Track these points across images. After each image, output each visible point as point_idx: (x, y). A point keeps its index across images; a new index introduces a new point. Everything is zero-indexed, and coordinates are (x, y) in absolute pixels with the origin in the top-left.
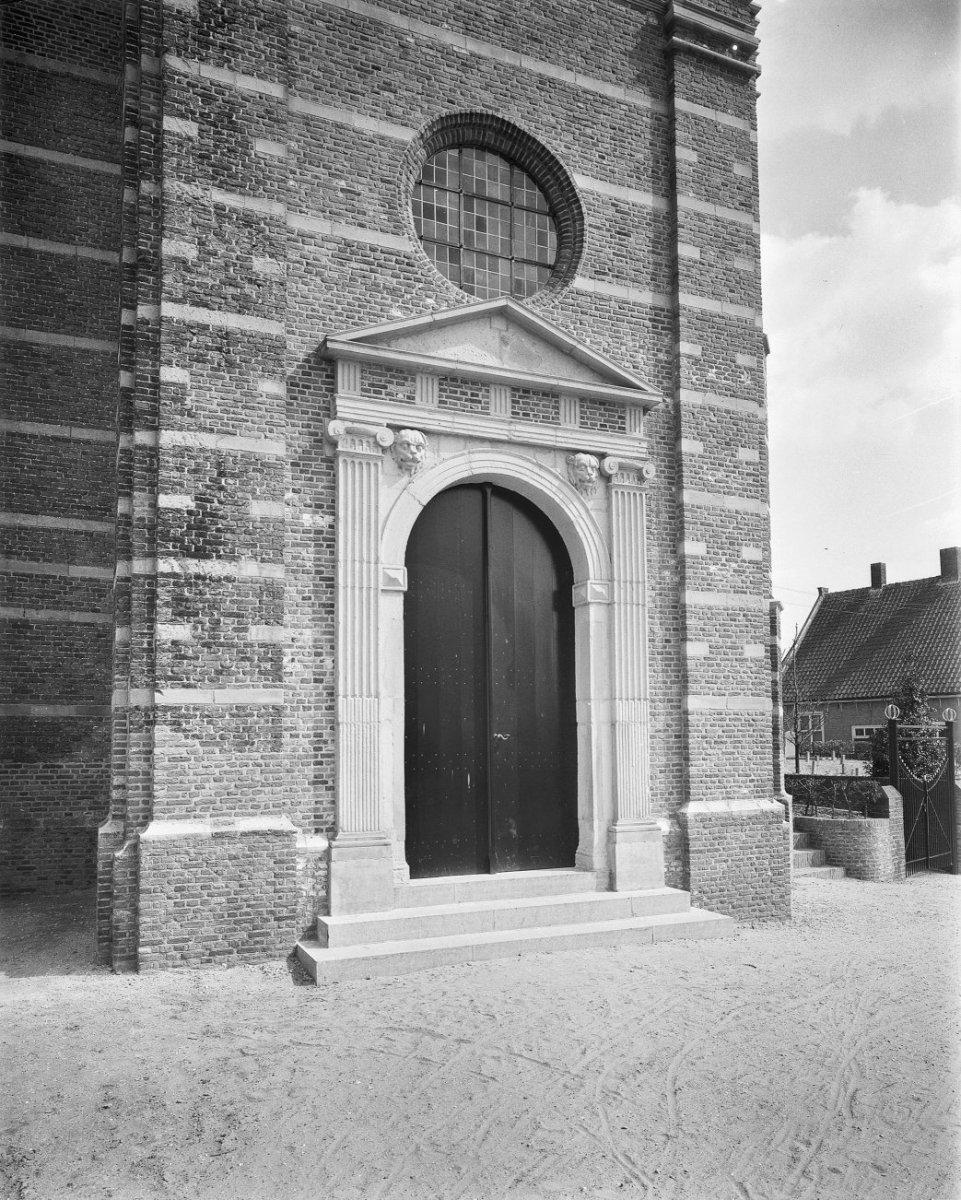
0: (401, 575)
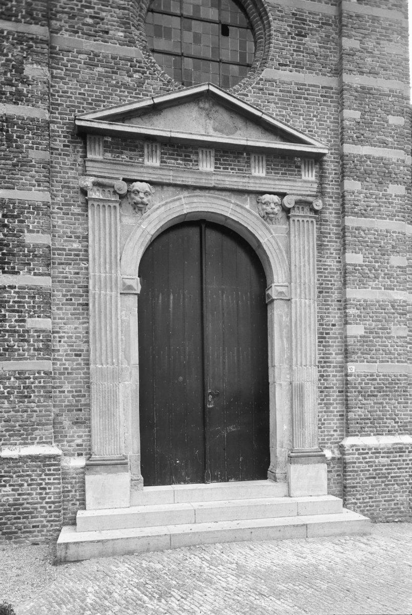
0: (136, 284)
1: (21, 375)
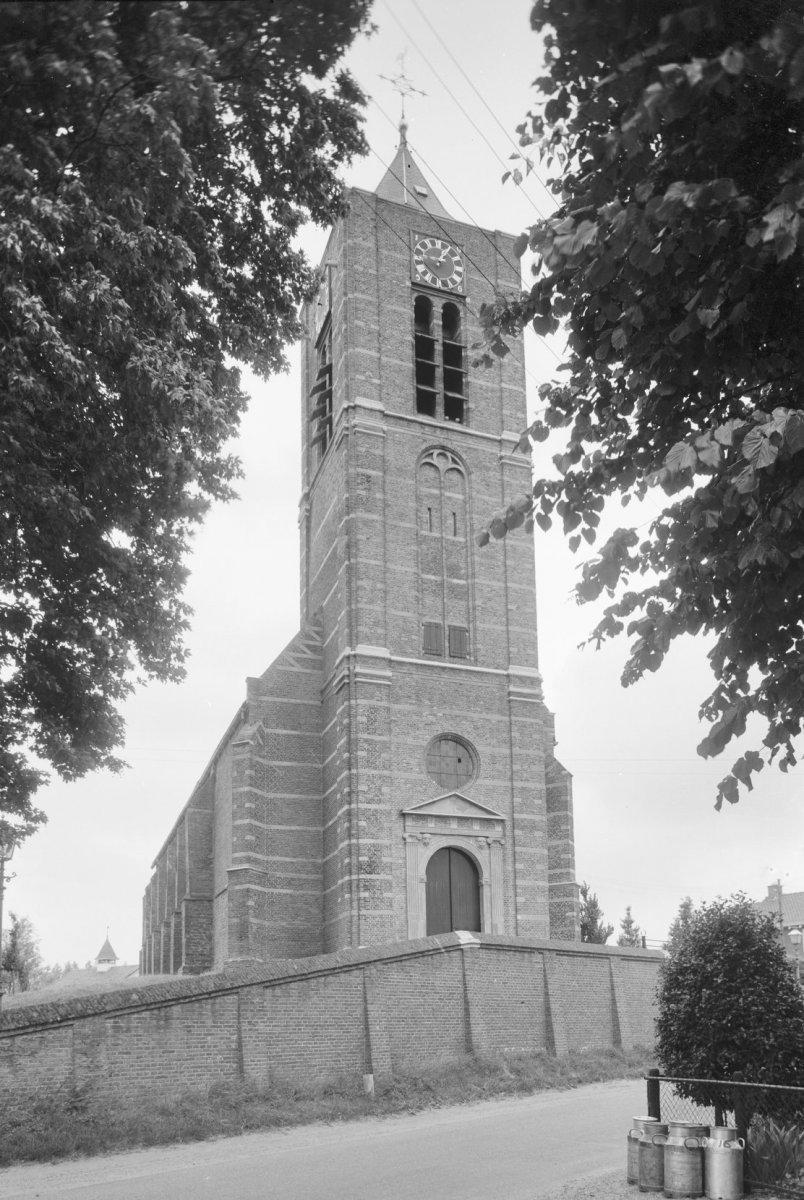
0: (425, 877)
1: (381, 916)
